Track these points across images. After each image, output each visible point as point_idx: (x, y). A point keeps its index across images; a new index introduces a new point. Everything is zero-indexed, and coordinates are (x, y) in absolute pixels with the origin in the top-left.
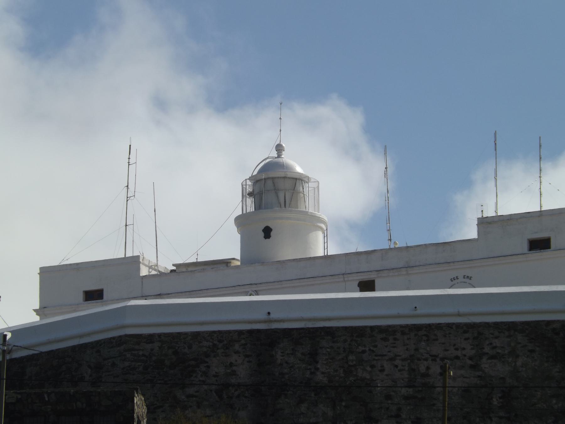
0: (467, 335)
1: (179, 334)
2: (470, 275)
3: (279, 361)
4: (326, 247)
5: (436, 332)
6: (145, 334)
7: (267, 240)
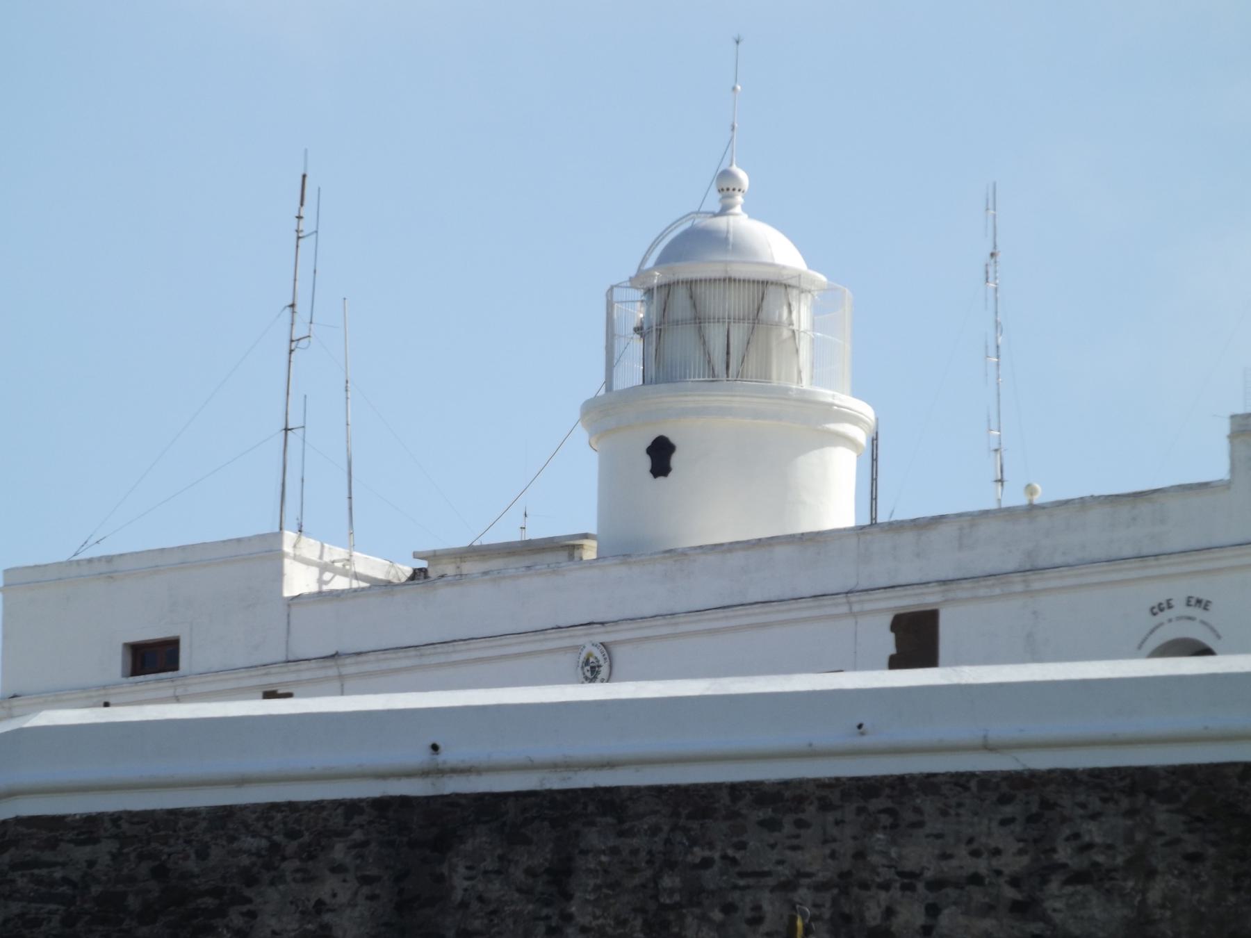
0: (1008, 810)
1: (174, 813)
2: (1204, 597)
3: (458, 896)
5: (918, 801)
6: (75, 815)
7: (661, 479)
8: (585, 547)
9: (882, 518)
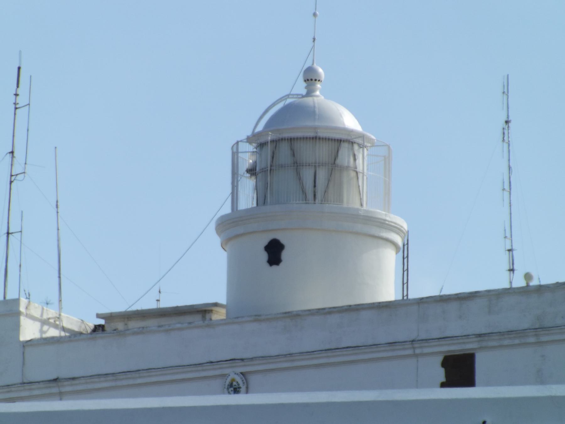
4: (405, 281)
7: (274, 267)
8: (214, 312)
9: (414, 294)
